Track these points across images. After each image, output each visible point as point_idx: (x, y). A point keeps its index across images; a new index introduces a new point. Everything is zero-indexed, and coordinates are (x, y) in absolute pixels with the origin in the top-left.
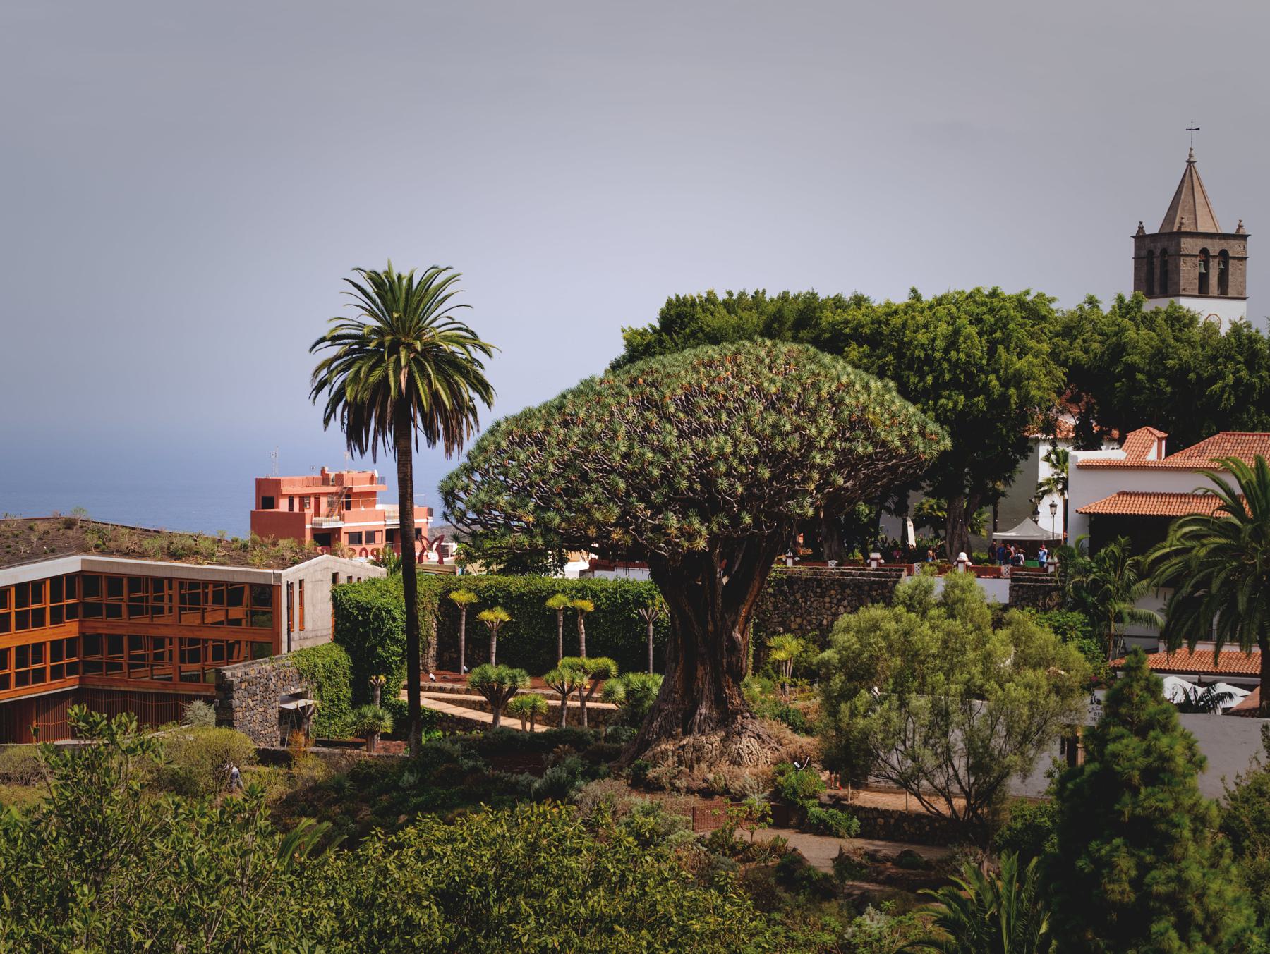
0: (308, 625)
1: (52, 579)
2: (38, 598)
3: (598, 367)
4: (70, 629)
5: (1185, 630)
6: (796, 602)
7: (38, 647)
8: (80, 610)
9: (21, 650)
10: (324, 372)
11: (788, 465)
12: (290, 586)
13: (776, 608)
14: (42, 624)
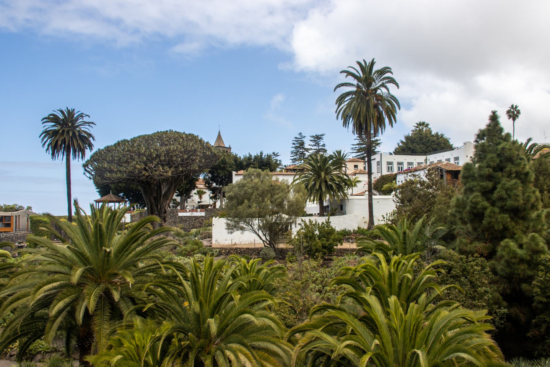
0: (21, 227)
10: (51, 116)
12: (16, 216)
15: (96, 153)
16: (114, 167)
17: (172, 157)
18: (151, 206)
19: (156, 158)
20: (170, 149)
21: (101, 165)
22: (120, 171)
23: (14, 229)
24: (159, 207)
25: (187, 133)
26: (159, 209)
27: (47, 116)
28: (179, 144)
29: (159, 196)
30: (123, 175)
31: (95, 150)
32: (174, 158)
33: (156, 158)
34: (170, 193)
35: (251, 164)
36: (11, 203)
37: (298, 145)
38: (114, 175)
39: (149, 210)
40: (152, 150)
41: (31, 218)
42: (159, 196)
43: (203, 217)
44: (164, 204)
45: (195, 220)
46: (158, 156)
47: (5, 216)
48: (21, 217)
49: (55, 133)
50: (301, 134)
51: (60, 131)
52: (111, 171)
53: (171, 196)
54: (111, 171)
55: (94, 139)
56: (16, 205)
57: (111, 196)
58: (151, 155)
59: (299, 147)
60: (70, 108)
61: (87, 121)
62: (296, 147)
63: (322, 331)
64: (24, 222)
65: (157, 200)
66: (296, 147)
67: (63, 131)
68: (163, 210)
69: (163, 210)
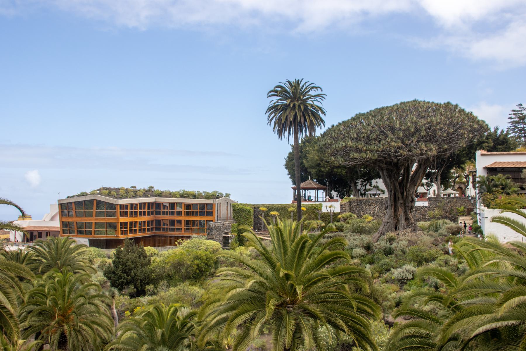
0: (222, 216)
1: (140, 203)
2: (136, 208)
3: (442, 103)
4: (146, 218)
5: (362, 306)
6: (362, 207)
7: (144, 222)
8: (154, 213)
9: (131, 223)
10: (279, 89)
11: (301, 20)
12: (218, 204)
13: (356, 209)
14: (127, 216)
15: (329, 130)
16: (361, 145)
17: (434, 131)
18: (395, 194)
19: (414, 133)
20: (432, 122)
21: (344, 144)
22: (372, 151)
23: (216, 219)
24: (405, 194)
25: (373, 109)
26: (405, 197)
27: (272, 89)
28: (441, 115)
29: (405, 181)
30: (374, 155)
31: (328, 125)
32: (439, 133)
33: (414, 133)
34: (419, 177)
35: (484, 142)
36: (211, 191)
37: (516, 120)
38: (363, 155)
39: (392, 199)
40: (409, 124)
41: (233, 206)
42: (405, 181)
43: (426, 207)
44: (412, 191)
45: (416, 211)
46: (417, 130)
47: (207, 204)
48: (221, 205)
49: (285, 108)
50: (521, 105)
51: (292, 105)
52: (358, 150)
53: (419, 181)
54: (358, 150)
55: (323, 112)
56: (217, 192)
57: (311, 182)
58: (408, 129)
59: (518, 122)
60: (292, 80)
61: (313, 94)
62: (512, 123)
63: (119, 323)
64: (224, 211)
65: (403, 185)
66: (512, 123)
67: (294, 105)
68: (410, 198)
69: (410, 198)
